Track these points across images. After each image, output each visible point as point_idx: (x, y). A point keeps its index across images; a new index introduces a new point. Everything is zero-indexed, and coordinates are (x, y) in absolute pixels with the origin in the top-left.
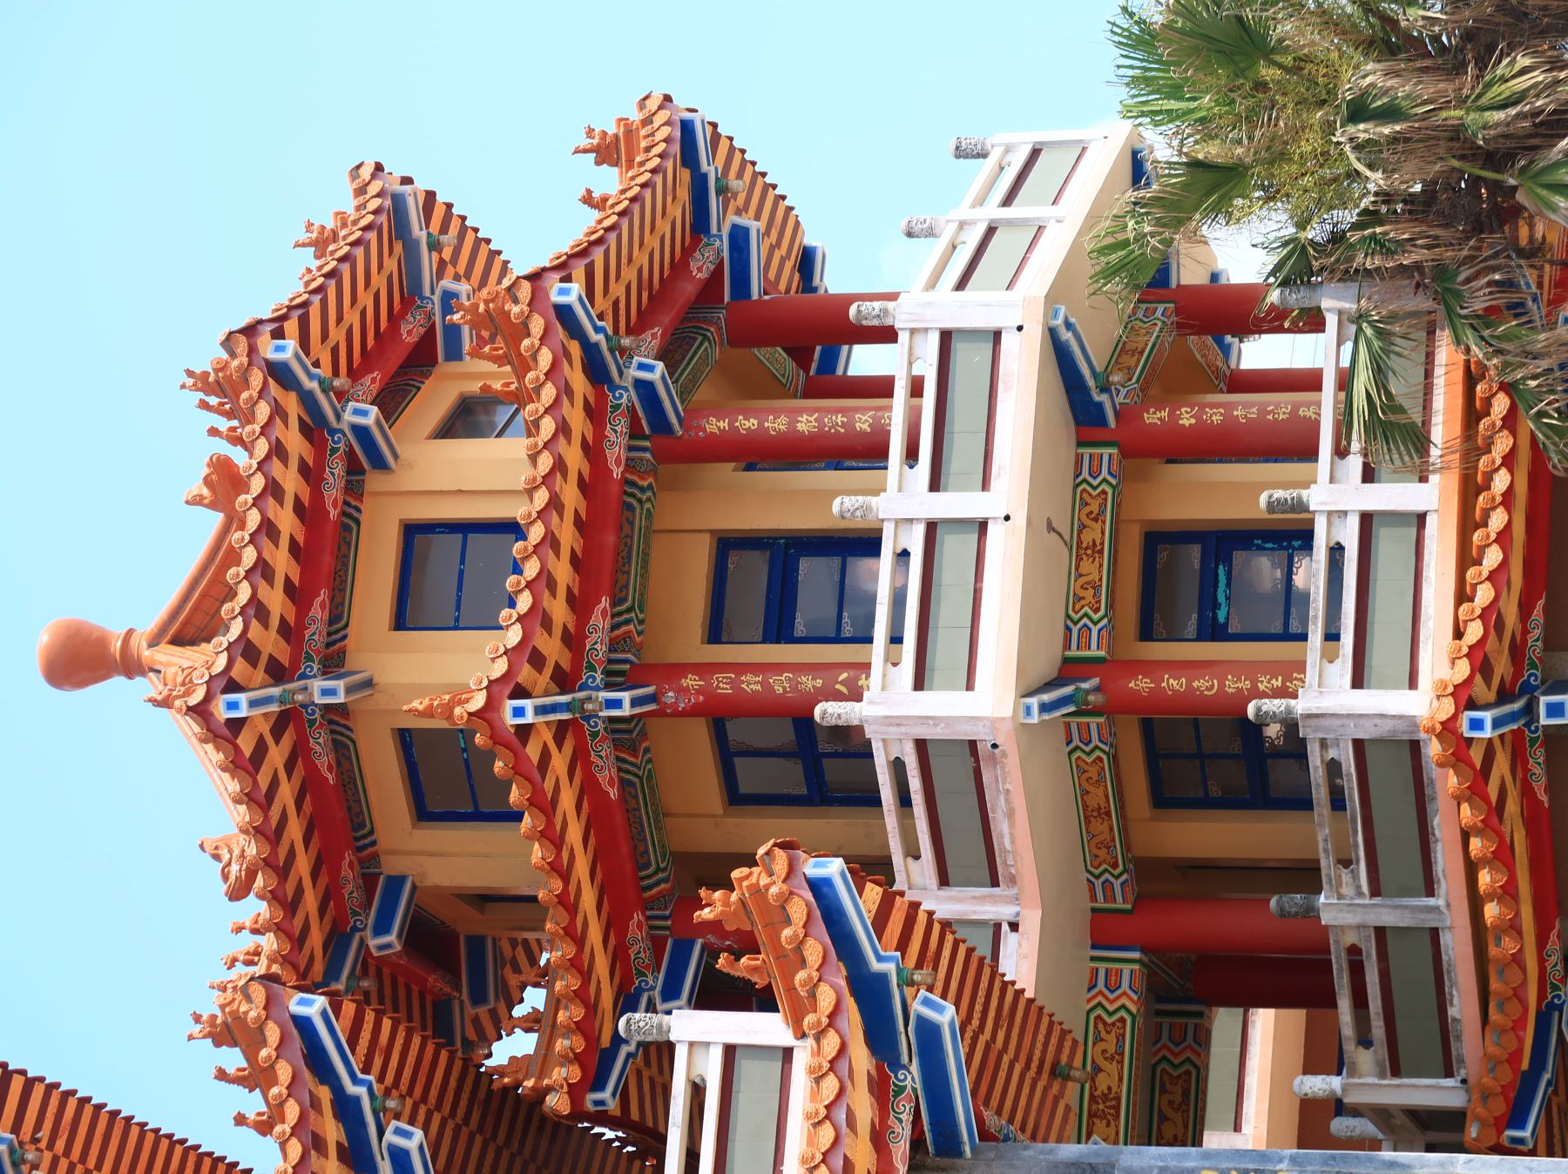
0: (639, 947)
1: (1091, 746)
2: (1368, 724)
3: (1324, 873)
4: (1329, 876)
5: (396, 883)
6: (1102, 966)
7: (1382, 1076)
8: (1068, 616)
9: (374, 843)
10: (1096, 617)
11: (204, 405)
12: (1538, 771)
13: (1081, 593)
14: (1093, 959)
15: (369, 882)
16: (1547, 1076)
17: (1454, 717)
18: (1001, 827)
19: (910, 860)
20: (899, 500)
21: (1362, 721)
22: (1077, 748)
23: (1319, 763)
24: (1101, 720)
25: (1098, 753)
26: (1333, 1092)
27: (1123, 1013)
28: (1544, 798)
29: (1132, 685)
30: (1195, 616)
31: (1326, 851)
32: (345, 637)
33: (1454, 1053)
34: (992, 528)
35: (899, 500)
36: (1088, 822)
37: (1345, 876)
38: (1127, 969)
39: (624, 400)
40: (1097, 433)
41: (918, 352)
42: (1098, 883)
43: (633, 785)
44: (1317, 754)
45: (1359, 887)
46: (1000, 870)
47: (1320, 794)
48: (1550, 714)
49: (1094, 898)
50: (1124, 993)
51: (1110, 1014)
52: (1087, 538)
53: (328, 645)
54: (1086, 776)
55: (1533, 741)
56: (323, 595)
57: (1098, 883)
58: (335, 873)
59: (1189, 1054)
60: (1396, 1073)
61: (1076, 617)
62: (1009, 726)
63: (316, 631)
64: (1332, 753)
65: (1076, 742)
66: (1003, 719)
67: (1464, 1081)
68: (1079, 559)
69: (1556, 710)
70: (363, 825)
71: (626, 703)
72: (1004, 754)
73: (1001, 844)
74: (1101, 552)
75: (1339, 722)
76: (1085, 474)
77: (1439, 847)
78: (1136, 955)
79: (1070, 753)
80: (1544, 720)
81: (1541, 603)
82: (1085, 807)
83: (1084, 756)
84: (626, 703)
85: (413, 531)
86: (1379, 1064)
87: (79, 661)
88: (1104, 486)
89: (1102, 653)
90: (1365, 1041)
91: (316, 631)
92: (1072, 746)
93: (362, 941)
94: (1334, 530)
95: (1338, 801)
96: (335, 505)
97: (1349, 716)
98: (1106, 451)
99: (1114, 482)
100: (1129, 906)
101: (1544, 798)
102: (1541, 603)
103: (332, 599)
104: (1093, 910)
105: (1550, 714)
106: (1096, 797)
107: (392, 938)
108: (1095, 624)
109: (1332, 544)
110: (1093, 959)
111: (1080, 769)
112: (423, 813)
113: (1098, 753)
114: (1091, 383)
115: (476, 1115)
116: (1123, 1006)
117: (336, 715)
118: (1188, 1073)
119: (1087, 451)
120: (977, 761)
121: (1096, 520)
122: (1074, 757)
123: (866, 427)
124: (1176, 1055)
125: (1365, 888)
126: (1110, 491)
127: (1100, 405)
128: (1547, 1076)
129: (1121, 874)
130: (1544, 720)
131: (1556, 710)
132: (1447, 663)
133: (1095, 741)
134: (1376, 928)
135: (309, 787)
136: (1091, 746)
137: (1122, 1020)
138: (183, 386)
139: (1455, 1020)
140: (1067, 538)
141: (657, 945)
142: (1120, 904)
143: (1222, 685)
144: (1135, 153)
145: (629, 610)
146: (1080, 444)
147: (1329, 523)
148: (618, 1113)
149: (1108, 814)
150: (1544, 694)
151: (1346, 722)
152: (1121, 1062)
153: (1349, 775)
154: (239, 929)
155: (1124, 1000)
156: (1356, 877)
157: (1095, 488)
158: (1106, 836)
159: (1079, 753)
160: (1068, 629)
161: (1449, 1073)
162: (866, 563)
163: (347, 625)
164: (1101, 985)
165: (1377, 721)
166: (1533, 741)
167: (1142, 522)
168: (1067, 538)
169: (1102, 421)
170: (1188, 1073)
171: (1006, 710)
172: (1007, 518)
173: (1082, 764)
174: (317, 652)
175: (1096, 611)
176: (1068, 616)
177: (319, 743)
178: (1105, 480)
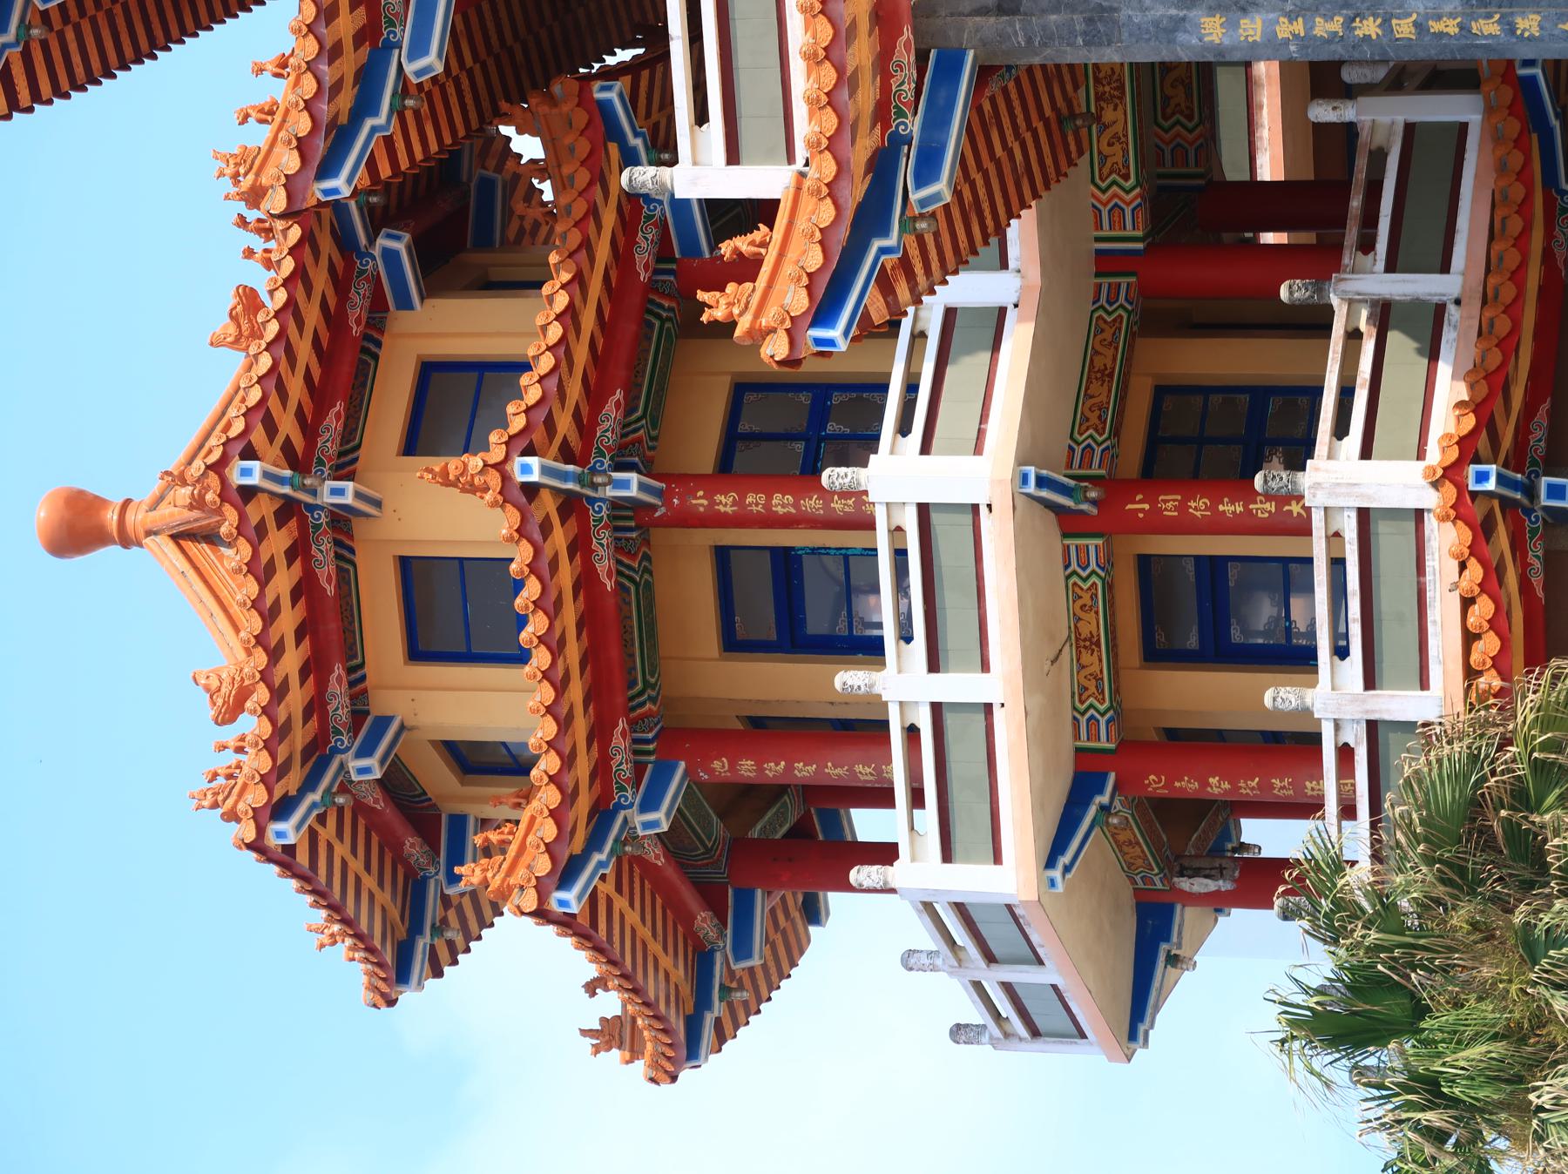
0: (622, 763)
1: (1088, 715)
5: (383, 722)
9: (363, 678)
10: (1100, 439)
11: (242, 222)
12: (1537, 565)
15: (358, 717)
19: (902, 643)
20: (902, 684)
22: (1074, 572)
24: (1099, 542)
25: (1094, 579)
28: (1540, 593)
30: (1195, 629)
32: (356, 459)
34: (996, 710)
35: (902, 684)
36: (1089, 381)
39: (658, 212)
42: (1083, 721)
43: (627, 590)
48: (1550, 496)
49: (1077, 737)
50: (1128, 204)
51: (1114, 183)
53: (341, 454)
54: (1080, 603)
55: (1534, 531)
56: (339, 407)
57: (1083, 721)
58: (322, 686)
63: (329, 442)
65: (1074, 565)
69: (1556, 492)
70: (355, 657)
71: (631, 485)
80: (1544, 501)
81: (1545, 407)
84: (631, 485)
85: (429, 370)
87: (80, 528)
89: (1102, 472)
91: (329, 442)
93: (342, 766)
96: (358, 322)
100: (1112, 746)
101: (1540, 593)
102: (1545, 407)
103: (347, 410)
104: (1078, 750)
105: (1550, 496)
107: (372, 762)
108: (1099, 445)
112: (417, 653)
117: (341, 520)
119: (1106, 281)
122: (1071, 582)
124: (1178, 135)
126: (1125, 316)
129: (1133, 189)
130: (1544, 501)
131: (1556, 492)
134: (1368, 722)
135: (304, 589)
136: (1088, 715)
137: (1121, 317)
138: (227, 197)
141: (639, 769)
142: (1104, 744)
144: (1132, 1036)
145: (639, 420)
148: (628, 78)
150: (1546, 474)
152: (1116, 349)
154: (259, 70)
157: (1091, 706)
158: (1119, 158)
159: (1074, 579)
160: (1071, 448)
162: (872, 599)
163: (358, 447)
174: (330, 460)
176: (1075, 708)
177: (323, 551)
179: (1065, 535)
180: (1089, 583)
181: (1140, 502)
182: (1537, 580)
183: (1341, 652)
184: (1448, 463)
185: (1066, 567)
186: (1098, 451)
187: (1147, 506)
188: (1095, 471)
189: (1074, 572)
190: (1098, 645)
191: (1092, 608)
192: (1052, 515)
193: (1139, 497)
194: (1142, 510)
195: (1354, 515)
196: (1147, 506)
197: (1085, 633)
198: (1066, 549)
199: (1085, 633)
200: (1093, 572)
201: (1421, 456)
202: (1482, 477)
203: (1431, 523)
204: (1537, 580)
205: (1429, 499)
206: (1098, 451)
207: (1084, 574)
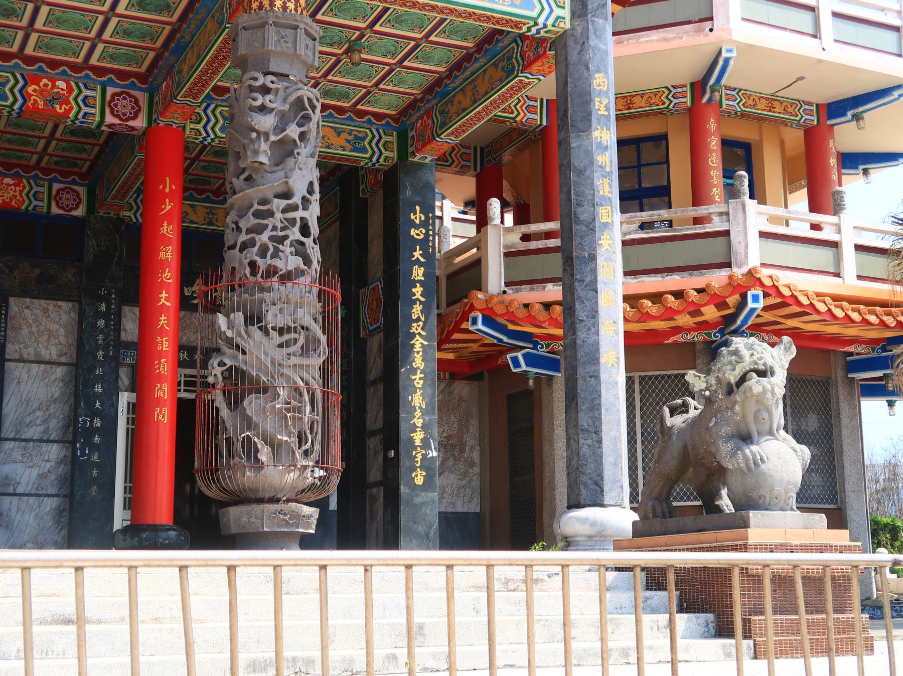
1: (672, 99)
2: (741, 238)
3: (639, 214)
4: (636, 217)
6: (538, 104)
7: (505, 247)
8: (740, 90)
10: (741, 104)
13: (751, 99)
14: (542, 100)
16: (505, 339)
17: (762, 284)
18: (655, 35)
21: (742, 235)
22: (670, 91)
23: (711, 211)
24: (689, 104)
25: (667, 102)
26: (493, 219)
27: (516, 113)
29: (712, 120)
31: (652, 215)
33: (522, 287)
37: (635, 226)
38: (537, 117)
40: (823, 114)
41: (889, 14)
44: (717, 210)
45: (629, 233)
46: (626, 36)
47: (701, 211)
52: (776, 104)
54: (653, 96)
57: (734, 93)
59: (456, 162)
60: (506, 255)
61: (740, 94)
62: (725, 36)
64: (716, 219)
65: (674, 91)
66: (730, 34)
67: (505, 292)
68: (767, 99)
72: (706, 35)
73: (643, 36)
74: (770, 111)
75: (740, 222)
76: (805, 107)
77: (660, 279)
78: (544, 123)
79: (667, 88)
82: (633, 96)
83: (665, 95)
86: (513, 245)
88: (800, 116)
89: (724, 106)
90: (525, 238)
92: (672, 89)
94: (829, 227)
95: (697, 221)
97: (746, 227)
98: (815, 118)
99: (671, 107)
101: (670, 341)
106: (637, 101)
109: (822, 225)
110: (542, 100)
111: (657, 93)
113: (667, 102)
114: (861, 109)
115: (124, 50)
116: (519, 114)
118: (447, 161)
120: (696, 22)
121: (784, 110)
122: (664, 90)
123: (162, 256)
125: (628, 237)
127: (844, 115)
128: (505, 339)
132: (786, 283)
133: (675, 101)
136: (672, 99)
137: (512, 112)
139: (544, 287)
140: (777, 94)
143: (714, 168)
146: (817, 105)
147: (832, 224)
149: (629, 108)
151: (741, 225)
153: (705, 228)
155: (522, 115)
156: (635, 232)
159: (667, 92)
161: (507, 284)
164: (529, 103)
165: (743, 244)
166: (709, 335)
167: (761, 142)
168: (777, 94)
169: (830, 117)
170: (447, 161)
171: (735, 37)
172: (824, 49)
173: (660, 94)
175: (743, 105)
176: (740, 90)
178: (671, 102)
179: (692, 84)
180: (665, 100)
181: (171, 188)
182: (680, 338)
183: (643, 226)
184: (762, 279)
185: (674, 87)
186: (735, 103)
187: (167, 190)
188: (724, 102)
189: (670, 91)
190: (628, 109)
191: (649, 104)
192: (700, 78)
193: (174, 187)
194: (165, 187)
195: (726, 228)
196: (167, 190)
197: (635, 100)
198: (685, 86)
199: (635, 100)
200: (671, 102)
201: (763, 265)
202: (756, 298)
203: (724, 273)
204: (680, 338)
205: (739, 272)
206: (735, 103)
207: (670, 97)
